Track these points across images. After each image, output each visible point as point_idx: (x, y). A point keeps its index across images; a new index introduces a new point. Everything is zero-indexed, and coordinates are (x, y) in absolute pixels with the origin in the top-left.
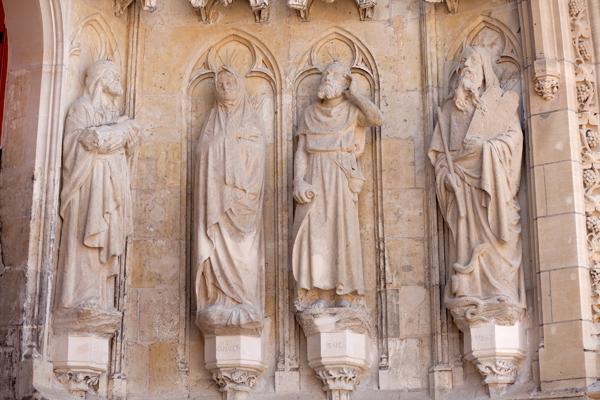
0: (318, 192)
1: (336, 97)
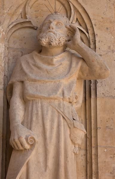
0: (39, 139)
1: (58, 47)
